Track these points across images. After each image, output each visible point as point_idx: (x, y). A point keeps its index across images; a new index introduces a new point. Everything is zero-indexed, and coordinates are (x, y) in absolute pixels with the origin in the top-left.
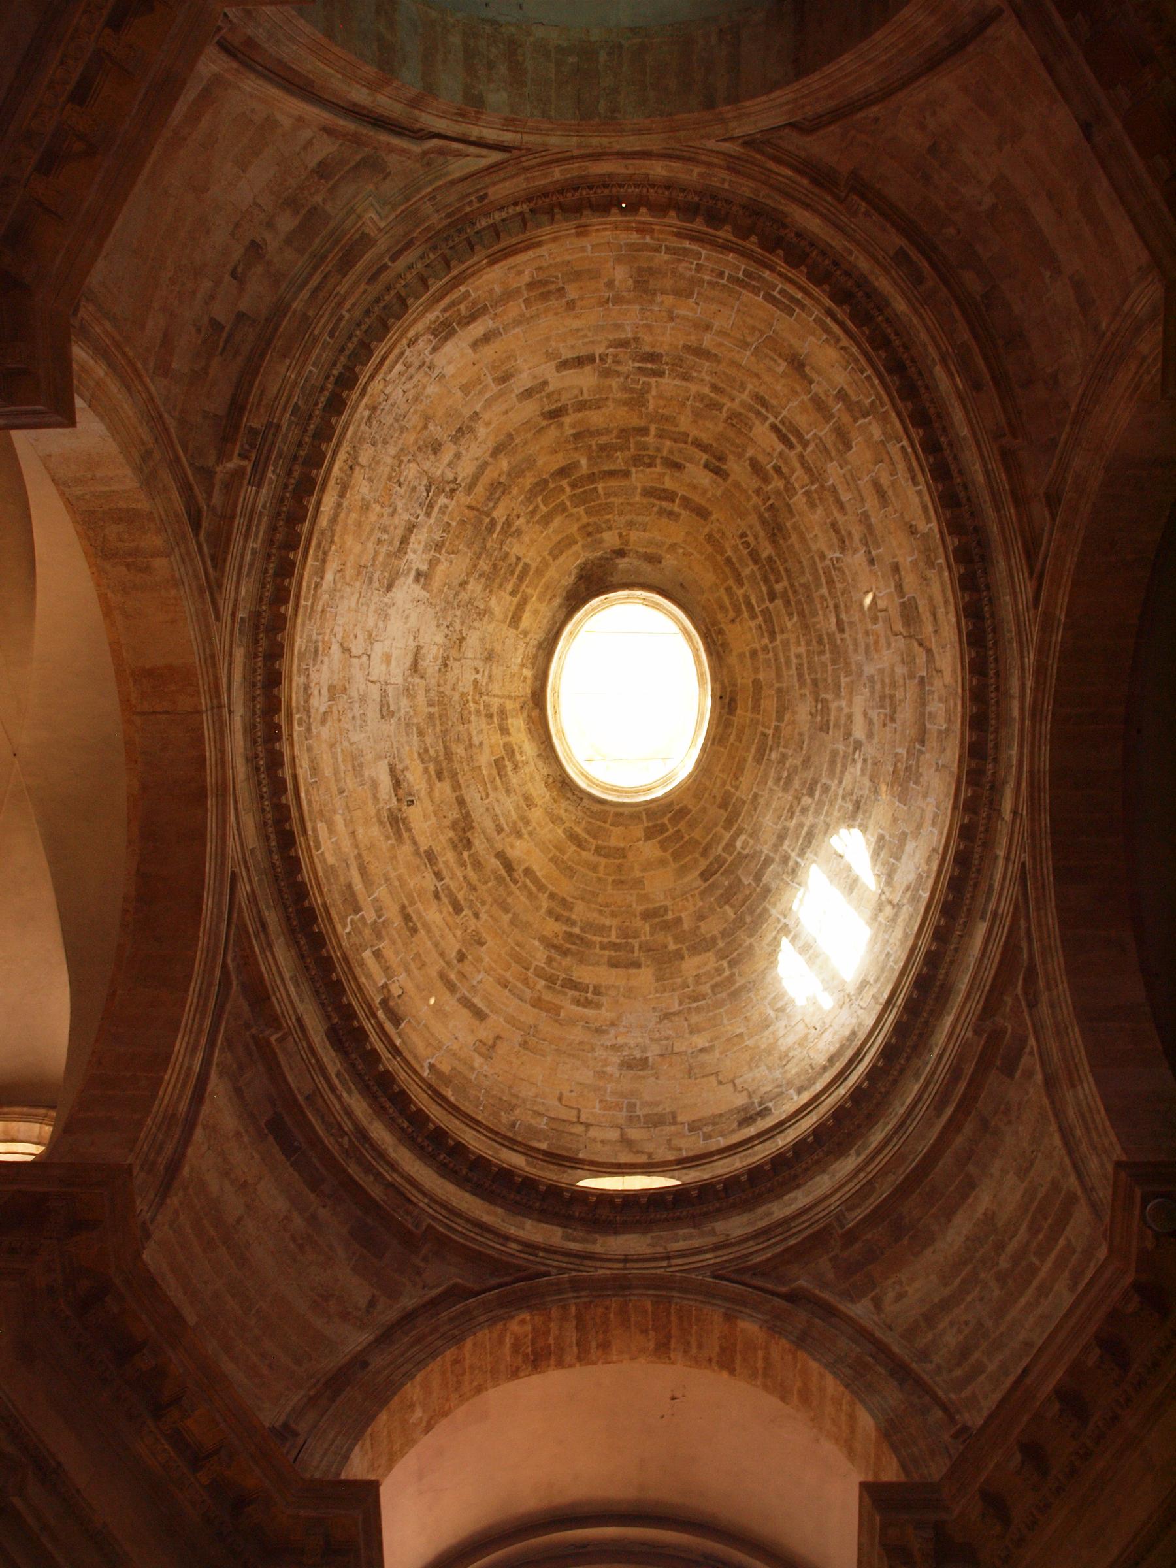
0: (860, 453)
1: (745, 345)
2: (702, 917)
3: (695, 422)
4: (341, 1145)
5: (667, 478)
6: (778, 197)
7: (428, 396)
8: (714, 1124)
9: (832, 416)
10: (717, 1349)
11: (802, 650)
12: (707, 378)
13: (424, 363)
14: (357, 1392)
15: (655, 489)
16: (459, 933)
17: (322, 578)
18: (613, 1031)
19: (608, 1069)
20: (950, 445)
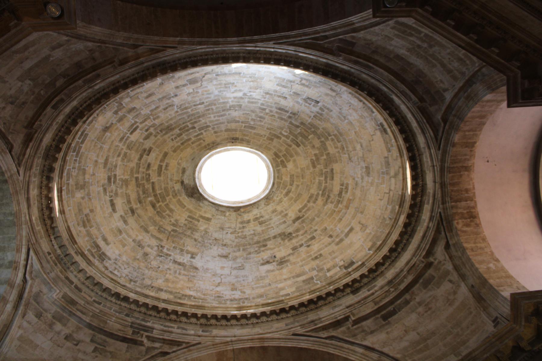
0: (136, 104)
1: (101, 148)
2: (313, 147)
3: (132, 161)
4: (393, 291)
5: (154, 169)
6: (40, 150)
7: (127, 259)
8: (387, 143)
9: (124, 115)
10: (466, 149)
11: (212, 116)
12: (115, 159)
13: (115, 263)
14: (482, 292)
15: (158, 172)
16: (322, 237)
17: (192, 296)
18: (357, 179)
19: (370, 181)
20: (123, 79)
